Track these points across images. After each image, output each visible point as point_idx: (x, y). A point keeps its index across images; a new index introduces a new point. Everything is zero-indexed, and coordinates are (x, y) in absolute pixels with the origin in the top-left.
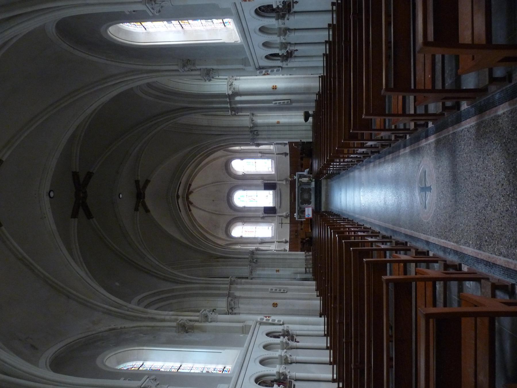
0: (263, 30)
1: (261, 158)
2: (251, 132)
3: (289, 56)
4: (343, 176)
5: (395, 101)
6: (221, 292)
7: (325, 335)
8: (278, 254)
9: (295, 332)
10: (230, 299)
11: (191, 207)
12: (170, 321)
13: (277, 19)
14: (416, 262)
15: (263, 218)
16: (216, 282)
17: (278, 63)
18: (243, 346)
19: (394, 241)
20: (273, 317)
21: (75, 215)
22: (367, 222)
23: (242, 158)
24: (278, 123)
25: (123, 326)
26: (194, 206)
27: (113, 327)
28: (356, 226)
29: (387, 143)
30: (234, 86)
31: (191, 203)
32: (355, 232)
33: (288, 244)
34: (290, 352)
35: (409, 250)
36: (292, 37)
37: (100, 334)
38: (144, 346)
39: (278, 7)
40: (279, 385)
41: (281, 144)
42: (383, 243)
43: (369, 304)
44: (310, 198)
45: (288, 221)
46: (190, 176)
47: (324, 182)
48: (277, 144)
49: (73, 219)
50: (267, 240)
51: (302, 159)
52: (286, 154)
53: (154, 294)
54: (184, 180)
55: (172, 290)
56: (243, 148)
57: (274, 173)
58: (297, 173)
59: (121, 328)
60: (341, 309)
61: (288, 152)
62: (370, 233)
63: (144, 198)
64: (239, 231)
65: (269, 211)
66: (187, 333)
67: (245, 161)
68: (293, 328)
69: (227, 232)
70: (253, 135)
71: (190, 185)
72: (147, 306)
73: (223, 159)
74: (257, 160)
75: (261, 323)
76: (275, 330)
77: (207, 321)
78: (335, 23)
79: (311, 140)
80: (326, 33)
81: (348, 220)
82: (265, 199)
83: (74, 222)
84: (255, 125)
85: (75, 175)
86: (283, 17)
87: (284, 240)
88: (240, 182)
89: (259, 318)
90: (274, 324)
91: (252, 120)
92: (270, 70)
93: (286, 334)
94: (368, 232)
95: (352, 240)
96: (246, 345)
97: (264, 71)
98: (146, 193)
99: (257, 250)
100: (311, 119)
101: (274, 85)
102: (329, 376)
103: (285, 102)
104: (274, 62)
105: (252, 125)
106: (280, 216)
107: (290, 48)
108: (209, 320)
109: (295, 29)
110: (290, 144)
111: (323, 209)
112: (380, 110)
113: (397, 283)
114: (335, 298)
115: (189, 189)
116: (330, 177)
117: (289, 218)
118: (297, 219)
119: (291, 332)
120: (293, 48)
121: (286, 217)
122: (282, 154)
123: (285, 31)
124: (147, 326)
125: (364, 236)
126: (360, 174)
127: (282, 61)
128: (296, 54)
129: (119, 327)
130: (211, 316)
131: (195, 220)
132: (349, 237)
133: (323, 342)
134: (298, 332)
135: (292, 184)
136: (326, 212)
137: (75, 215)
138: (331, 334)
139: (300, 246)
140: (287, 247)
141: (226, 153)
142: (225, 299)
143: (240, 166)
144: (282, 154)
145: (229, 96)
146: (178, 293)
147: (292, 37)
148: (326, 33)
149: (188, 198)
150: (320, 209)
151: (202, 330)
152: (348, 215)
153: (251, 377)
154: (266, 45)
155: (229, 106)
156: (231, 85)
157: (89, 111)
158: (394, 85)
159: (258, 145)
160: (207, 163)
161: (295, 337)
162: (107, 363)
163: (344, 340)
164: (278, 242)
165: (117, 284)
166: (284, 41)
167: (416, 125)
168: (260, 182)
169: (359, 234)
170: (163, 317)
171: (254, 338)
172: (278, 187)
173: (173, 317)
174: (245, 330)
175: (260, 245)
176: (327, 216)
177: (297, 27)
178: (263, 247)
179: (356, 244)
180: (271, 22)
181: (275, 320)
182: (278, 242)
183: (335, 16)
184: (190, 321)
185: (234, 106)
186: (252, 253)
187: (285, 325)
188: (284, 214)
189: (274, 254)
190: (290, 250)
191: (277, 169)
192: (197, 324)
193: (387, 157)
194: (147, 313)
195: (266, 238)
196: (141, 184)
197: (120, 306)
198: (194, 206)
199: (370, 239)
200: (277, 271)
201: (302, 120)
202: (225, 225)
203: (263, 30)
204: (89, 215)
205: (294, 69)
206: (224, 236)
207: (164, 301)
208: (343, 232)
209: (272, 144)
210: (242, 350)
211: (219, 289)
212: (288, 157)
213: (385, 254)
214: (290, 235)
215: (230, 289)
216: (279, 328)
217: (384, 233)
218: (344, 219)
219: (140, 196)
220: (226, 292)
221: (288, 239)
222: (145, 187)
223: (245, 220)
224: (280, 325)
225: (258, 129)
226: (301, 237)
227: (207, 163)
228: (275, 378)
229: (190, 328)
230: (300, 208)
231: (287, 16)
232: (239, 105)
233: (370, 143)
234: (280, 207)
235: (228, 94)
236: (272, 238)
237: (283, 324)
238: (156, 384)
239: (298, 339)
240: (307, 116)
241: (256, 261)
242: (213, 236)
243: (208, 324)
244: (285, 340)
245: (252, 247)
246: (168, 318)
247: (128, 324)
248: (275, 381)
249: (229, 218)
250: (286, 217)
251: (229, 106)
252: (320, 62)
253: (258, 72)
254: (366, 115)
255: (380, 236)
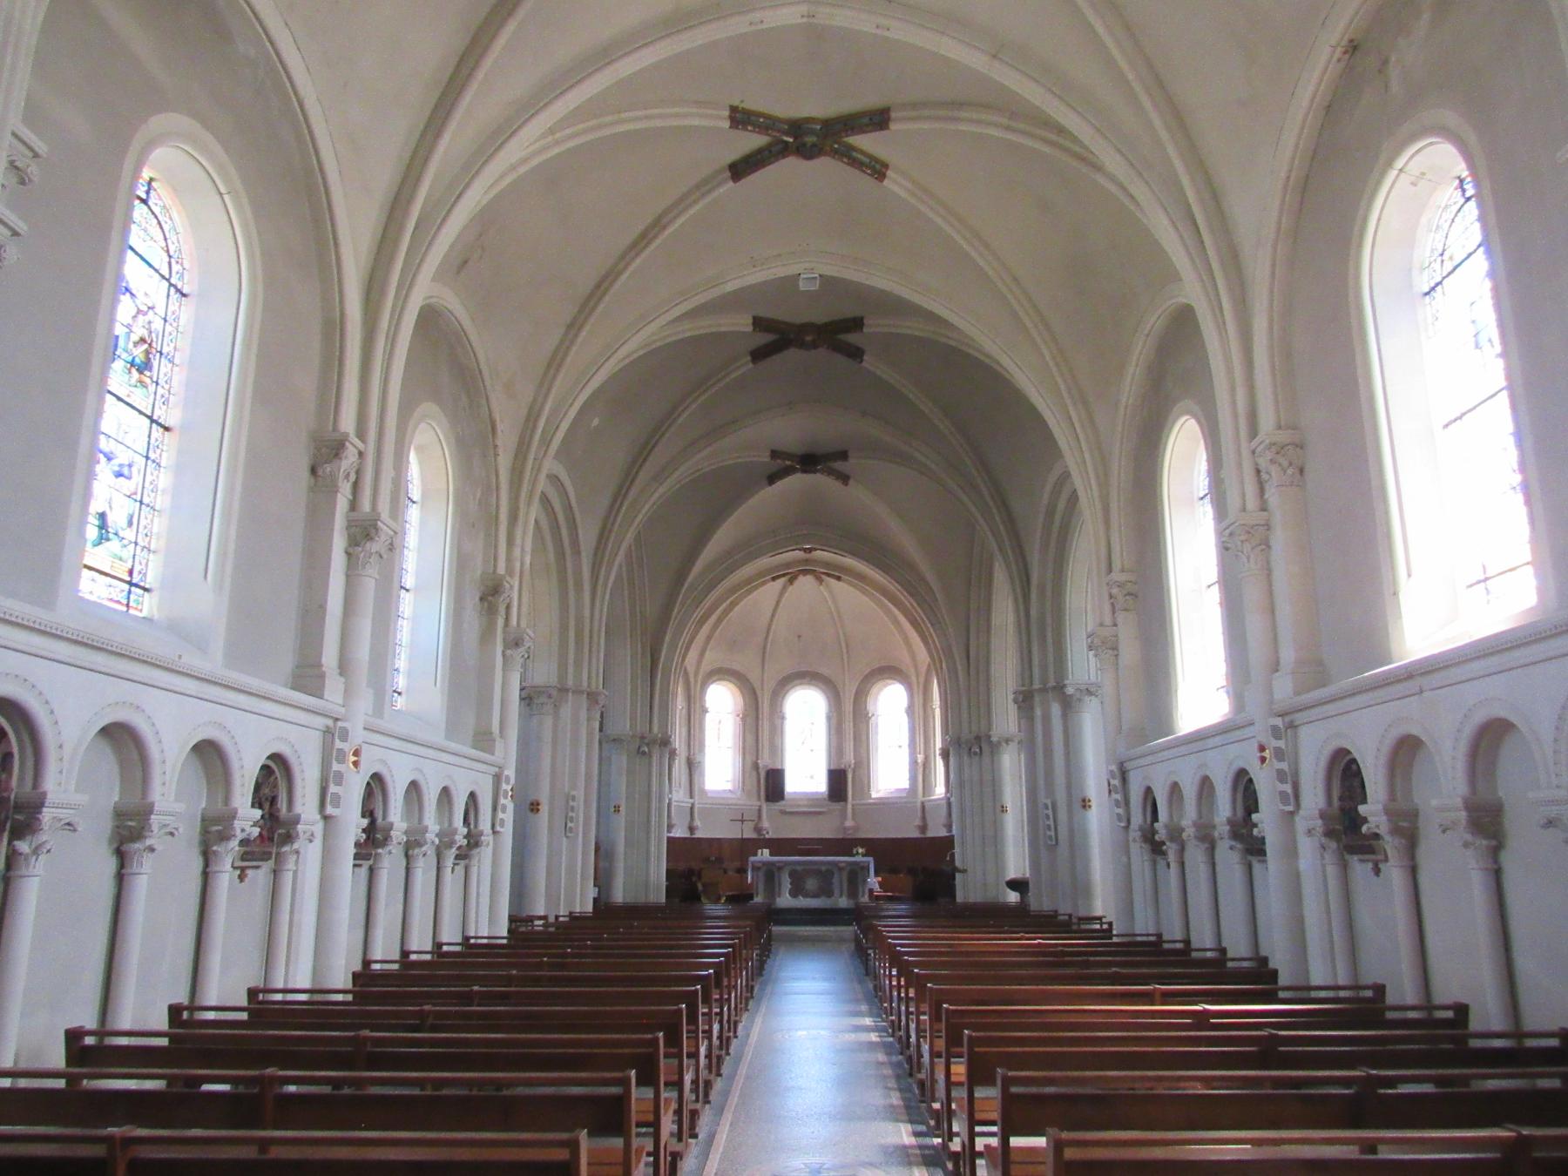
0: (1206, 785)
1: (913, 763)
2: (978, 738)
3: (1157, 849)
4: (860, 982)
5: (988, 1095)
6: (571, 670)
7: (466, 939)
8: (660, 809)
9: (475, 862)
10: (554, 693)
11: (783, 580)
12: (509, 560)
13: (1230, 822)
14: (655, 1153)
15: (756, 766)
16: (594, 655)
17: (1137, 819)
18: (448, 737)
19: (698, 1106)
20: (510, 807)
21: (759, 323)
22: (744, 1044)
23: (910, 711)
24: (1003, 810)
25: (500, 451)
26: (784, 588)
27: (500, 427)
28: (725, 1034)
29: (928, 1094)
30: (1087, 699)
31: (791, 581)
32: (721, 1014)
33: (687, 835)
34: (431, 852)
35: (680, 1140)
36: (1196, 856)
37: (484, 402)
38: (456, 503)
39: (1255, 825)
40: (364, 831)
41: (950, 815)
42: (695, 1082)
43: (572, 1043)
44: (806, 895)
45: (749, 834)
46: (861, 577)
47: (848, 931)
48: (949, 804)
49: (750, 321)
50: (696, 778)
51: (911, 871)
52: (923, 828)
53: (568, 508)
54: (849, 561)
55: (577, 552)
56: (938, 712)
57: (874, 795)
58: (871, 859)
59: (496, 447)
60: (537, 981)
61: (930, 834)
62: (715, 1052)
63: (805, 471)
64: (722, 703)
65: (773, 784)
66: (481, 599)
67: (904, 720)
68: (484, 855)
69: (720, 673)
70: (969, 745)
71: (839, 578)
72: (545, 499)
73: (904, 659)
74: (905, 751)
75: (497, 779)
76: (481, 811)
77: (506, 646)
78: (1230, 964)
79: (960, 898)
80: (1209, 942)
81: (747, 1000)
82: (805, 774)
83: (743, 323)
84: (995, 748)
85: (856, 324)
86: (1235, 835)
87: (697, 823)
88: (848, 707)
89: (510, 772)
90: (495, 809)
91: (1007, 741)
92: (1118, 797)
93: (473, 841)
94: (721, 1048)
95: (703, 1009)
96: (453, 746)
97: (1116, 782)
98: (818, 475)
99: (673, 753)
100: (1013, 897)
101: (1093, 804)
102: (377, 953)
103: (1053, 830)
104: (1140, 810)
105: (994, 739)
106: (760, 811)
107: (1171, 849)
108: (509, 652)
109: (1214, 865)
110: (948, 843)
111: (776, 929)
112: (979, 1074)
113: (622, 1102)
114: (563, 966)
115: (828, 575)
116: (861, 953)
117: (754, 836)
118: (752, 859)
119: (475, 851)
120: (1172, 857)
121: (758, 829)
122: (924, 818)
123: (1207, 839)
124: (498, 507)
125: (710, 1038)
126: (867, 1028)
127: (1141, 829)
128: (1161, 863)
129: (499, 443)
130: (518, 655)
131: (749, 592)
132: (707, 1000)
133: (450, 935)
134: (474, 870)
135: (843, 846)
136: (770, 937)
137: (759, 323)
138: (470, 955)
139: (682, 866)
140: (680, 832)
141: (923, 669)
142: (554, 680)
143: (890, 705)
144: (924, 818)
145: (1060, 688)
146: (569, 564)
147: (1196, 856)
148: (1209, 942)
149: (805, 572)
150: (778, 923)
151: (487, 635)
152: (760, 1000)
153: (384, 762)
154: (1175, 789)
155: (1037, 686)
156: (1089, 693)
157: (1005, 361)
158: (1018, 1096)
159: (945, 755)
160: (896, 622)
161: (463, 863)
162: (423, 426)
163: (476, 988)
164: (692, 808)
165: (596, 422)
166: (1184, 835)
167: (956, 1154)
168: (849, 758)
169: (716, 1027)
170: (518, 541)
171: (466, 762)
172: (837, 806)
173: (518, 565)
174: (483, 740)
175: (683, 761)
176: (762, 935)
177: (1218, 869)
178: (679, 766)
179: (693, 1019)
180: (1224, 808)
181: (504, 811)
182: (692, 808)
183: (1245, 964)
184: (508, 607)
185: (1037, 699)
186: (665, 742)
187: (491, 838)
188: (766, 824)
189: (661, 800)
190: (670, 840)
191: (885, 805)
192: (500, 622)
193: (898, 1094)
194: (529, 504)
195: (702, 774)
196: (838, 465)
197: (546, 442)
198: (784, 588)
199: (703, 1050)
200: (617, 809)
201: (1012, 873)
202: (736, 667)
203: (1206, 785)
204: (758, 355)
205: (1125, 859)
206: (706, 666)
207: (558, 534)
208: (718, 984)
209: (948, 790)
210: (439, 738)
211: (578, 664)
212: (915, 834)
213: (647, 1125)
214: (710, 841)
215: (577, 692)
216: (485, 824)
217: (718, 1085)
218: (750, 989)
219: (809, 461)
220: (570, 683)
221: (698, 835)
222: (831, 472)
223: (749, 720)
224: (493, 826)
225: (986, 759)
226: (700, 869)
227: (896, 622)
228: (380, 820)
229: (490, 603)
230: (780, 868)
231: (1239, 846)
232: (1038, 712)
233: (926, 1048)
234: (783, 812)
235: (1064, 686)
236: (703, 792)
237: (495, 832)
238: (382, 552)
239: (460, 870)
240: (1017, 885)
241: (644, 753)
242: (709, 638)
243: (499, 648)
244: (461, 840)
245: (678, 742)
246: (517, 552)
247: (504, 462)
248: (373, 822)
249: (754, 677)
250: (758, 829)
251: (1037, 686)
252: (1143, 926)
253: (1114, 767)
254: (970, 1037)
255: (698, 1106)
